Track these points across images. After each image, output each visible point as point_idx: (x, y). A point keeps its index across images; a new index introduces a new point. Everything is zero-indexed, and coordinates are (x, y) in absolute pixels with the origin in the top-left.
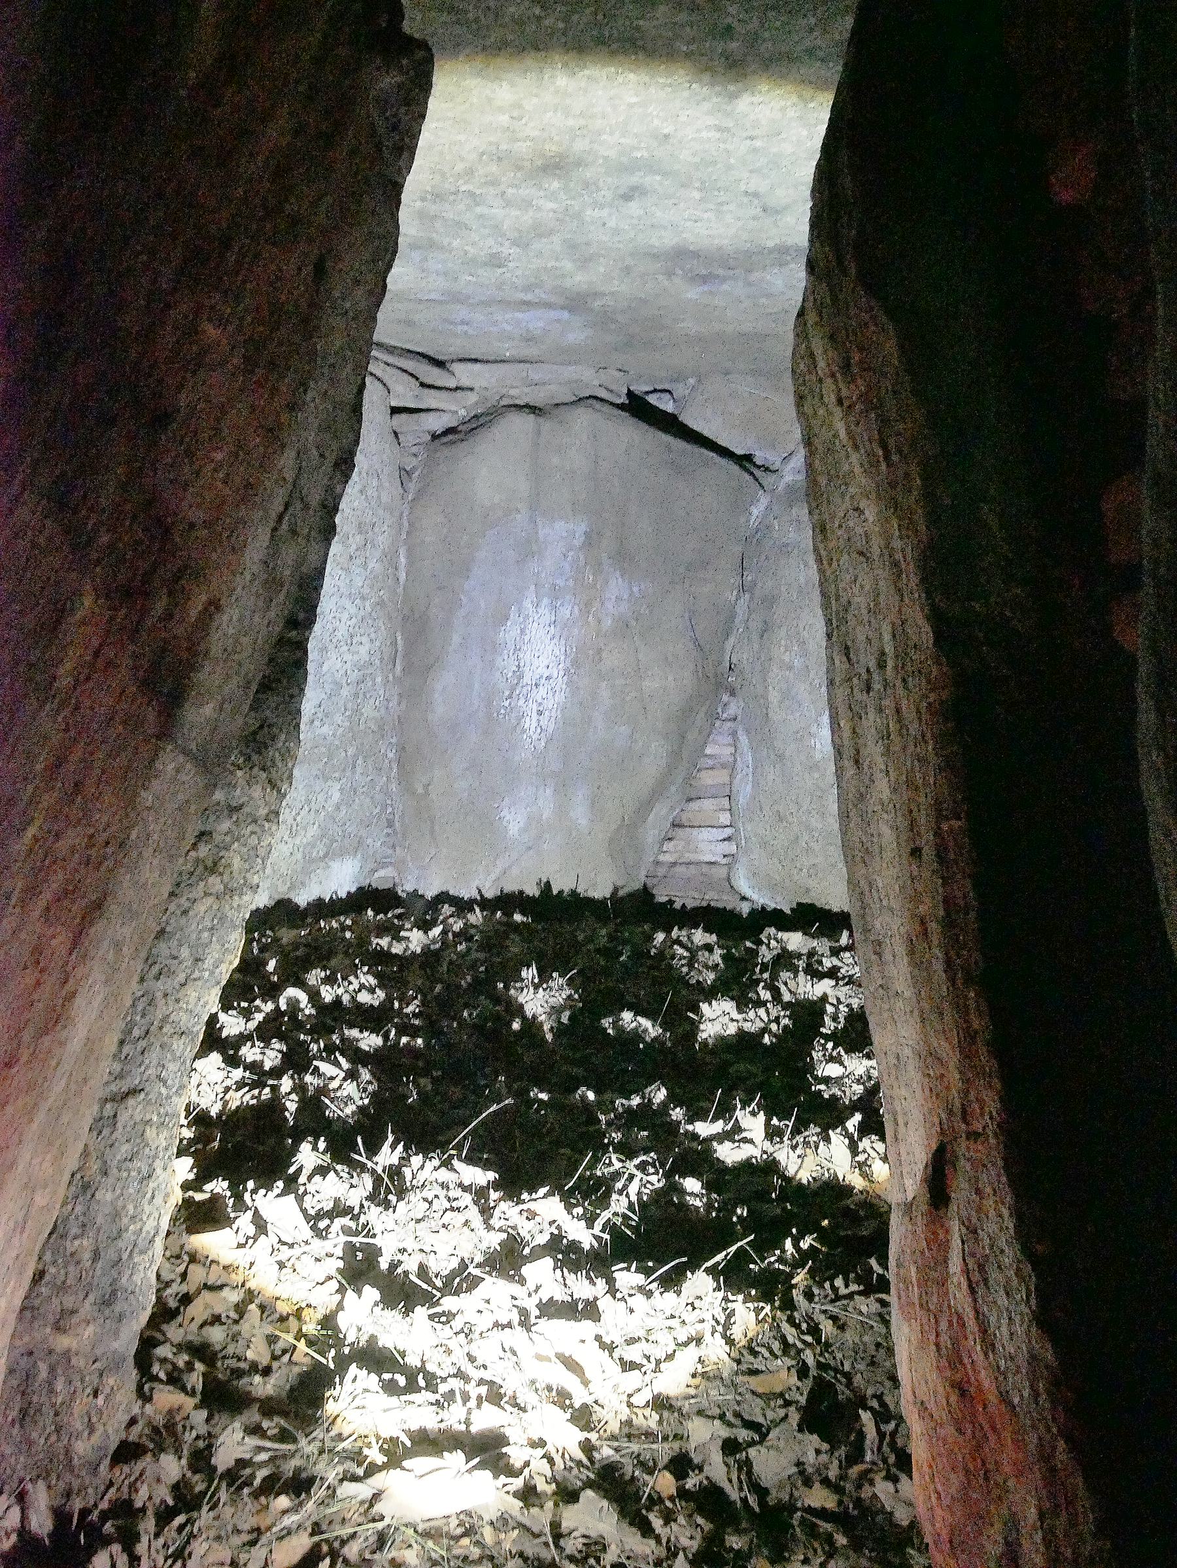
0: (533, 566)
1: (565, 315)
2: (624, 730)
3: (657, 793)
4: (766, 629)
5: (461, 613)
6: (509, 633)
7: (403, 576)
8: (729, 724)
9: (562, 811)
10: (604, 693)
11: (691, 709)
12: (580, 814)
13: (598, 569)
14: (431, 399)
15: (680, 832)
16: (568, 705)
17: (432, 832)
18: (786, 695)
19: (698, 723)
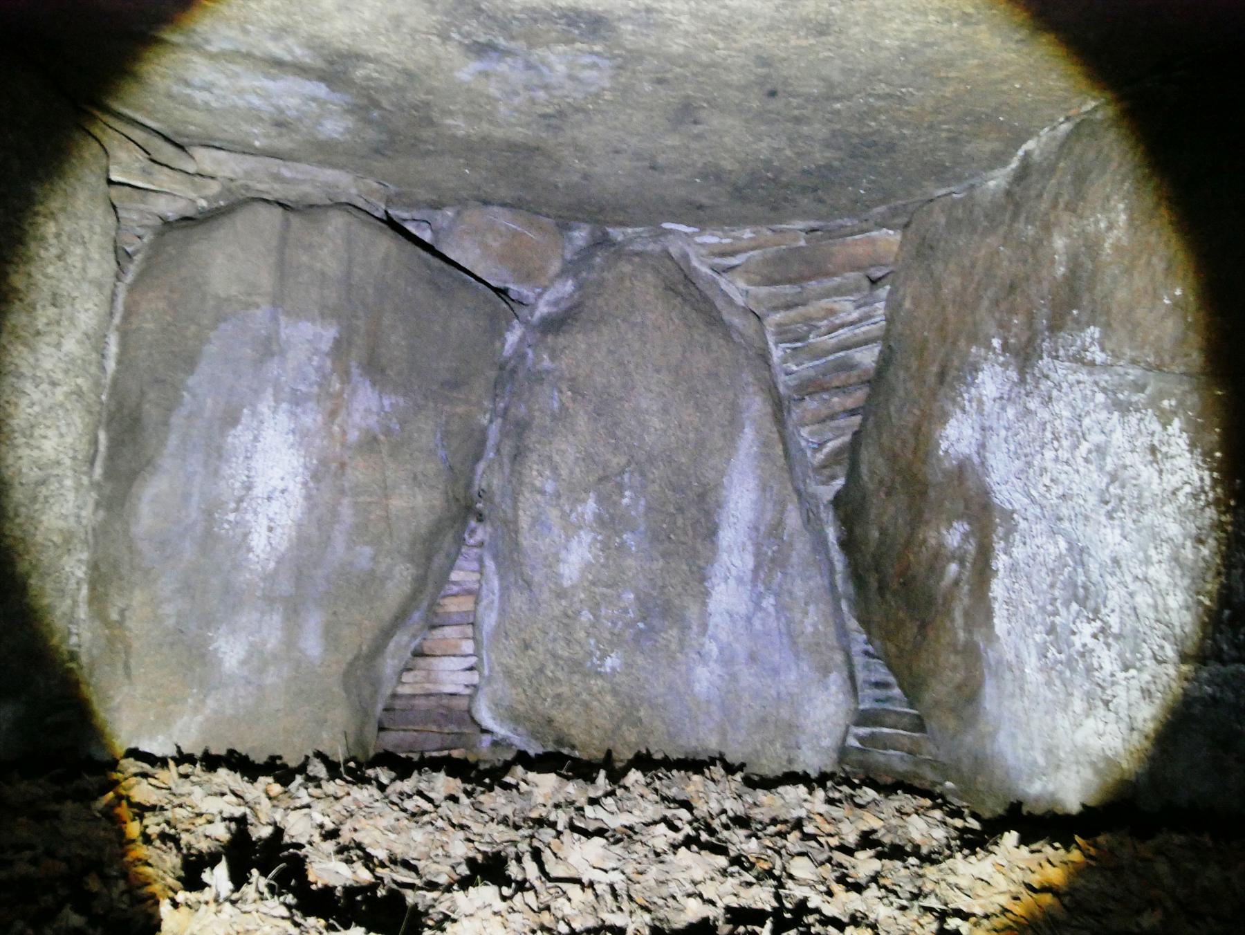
0: (272, 368)
1: (321, 90)
2: (368, 551)
3: (400, 619)
4: (518, 456)
5: (184, 411)
6: (239, 437)
7: (111, 365)
8: (476, 550)
9: (290, 642)
10: (346, 511)
11: (805, 212)
12: (312, 645)
13: (346, 376)
14: (164, 180)
15: (421, 662)
16: (305, 522)
17: (127, 667)
18: (536, 521)
19: (446, 545)
